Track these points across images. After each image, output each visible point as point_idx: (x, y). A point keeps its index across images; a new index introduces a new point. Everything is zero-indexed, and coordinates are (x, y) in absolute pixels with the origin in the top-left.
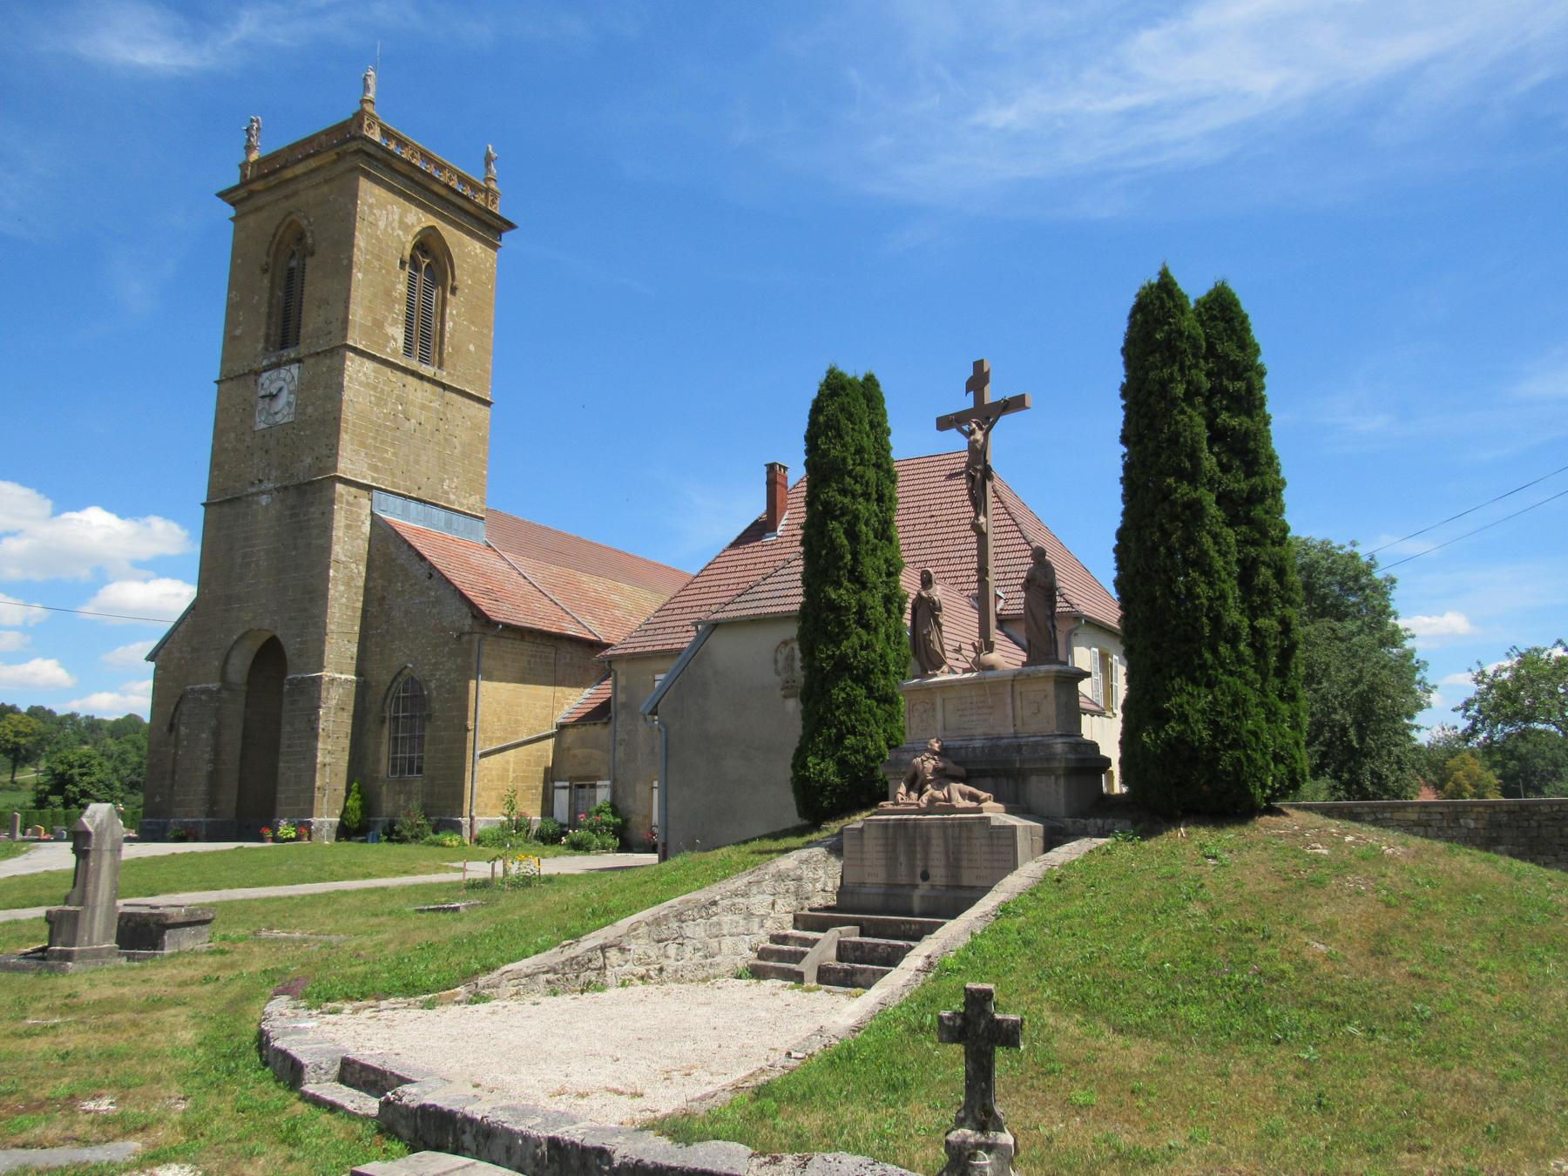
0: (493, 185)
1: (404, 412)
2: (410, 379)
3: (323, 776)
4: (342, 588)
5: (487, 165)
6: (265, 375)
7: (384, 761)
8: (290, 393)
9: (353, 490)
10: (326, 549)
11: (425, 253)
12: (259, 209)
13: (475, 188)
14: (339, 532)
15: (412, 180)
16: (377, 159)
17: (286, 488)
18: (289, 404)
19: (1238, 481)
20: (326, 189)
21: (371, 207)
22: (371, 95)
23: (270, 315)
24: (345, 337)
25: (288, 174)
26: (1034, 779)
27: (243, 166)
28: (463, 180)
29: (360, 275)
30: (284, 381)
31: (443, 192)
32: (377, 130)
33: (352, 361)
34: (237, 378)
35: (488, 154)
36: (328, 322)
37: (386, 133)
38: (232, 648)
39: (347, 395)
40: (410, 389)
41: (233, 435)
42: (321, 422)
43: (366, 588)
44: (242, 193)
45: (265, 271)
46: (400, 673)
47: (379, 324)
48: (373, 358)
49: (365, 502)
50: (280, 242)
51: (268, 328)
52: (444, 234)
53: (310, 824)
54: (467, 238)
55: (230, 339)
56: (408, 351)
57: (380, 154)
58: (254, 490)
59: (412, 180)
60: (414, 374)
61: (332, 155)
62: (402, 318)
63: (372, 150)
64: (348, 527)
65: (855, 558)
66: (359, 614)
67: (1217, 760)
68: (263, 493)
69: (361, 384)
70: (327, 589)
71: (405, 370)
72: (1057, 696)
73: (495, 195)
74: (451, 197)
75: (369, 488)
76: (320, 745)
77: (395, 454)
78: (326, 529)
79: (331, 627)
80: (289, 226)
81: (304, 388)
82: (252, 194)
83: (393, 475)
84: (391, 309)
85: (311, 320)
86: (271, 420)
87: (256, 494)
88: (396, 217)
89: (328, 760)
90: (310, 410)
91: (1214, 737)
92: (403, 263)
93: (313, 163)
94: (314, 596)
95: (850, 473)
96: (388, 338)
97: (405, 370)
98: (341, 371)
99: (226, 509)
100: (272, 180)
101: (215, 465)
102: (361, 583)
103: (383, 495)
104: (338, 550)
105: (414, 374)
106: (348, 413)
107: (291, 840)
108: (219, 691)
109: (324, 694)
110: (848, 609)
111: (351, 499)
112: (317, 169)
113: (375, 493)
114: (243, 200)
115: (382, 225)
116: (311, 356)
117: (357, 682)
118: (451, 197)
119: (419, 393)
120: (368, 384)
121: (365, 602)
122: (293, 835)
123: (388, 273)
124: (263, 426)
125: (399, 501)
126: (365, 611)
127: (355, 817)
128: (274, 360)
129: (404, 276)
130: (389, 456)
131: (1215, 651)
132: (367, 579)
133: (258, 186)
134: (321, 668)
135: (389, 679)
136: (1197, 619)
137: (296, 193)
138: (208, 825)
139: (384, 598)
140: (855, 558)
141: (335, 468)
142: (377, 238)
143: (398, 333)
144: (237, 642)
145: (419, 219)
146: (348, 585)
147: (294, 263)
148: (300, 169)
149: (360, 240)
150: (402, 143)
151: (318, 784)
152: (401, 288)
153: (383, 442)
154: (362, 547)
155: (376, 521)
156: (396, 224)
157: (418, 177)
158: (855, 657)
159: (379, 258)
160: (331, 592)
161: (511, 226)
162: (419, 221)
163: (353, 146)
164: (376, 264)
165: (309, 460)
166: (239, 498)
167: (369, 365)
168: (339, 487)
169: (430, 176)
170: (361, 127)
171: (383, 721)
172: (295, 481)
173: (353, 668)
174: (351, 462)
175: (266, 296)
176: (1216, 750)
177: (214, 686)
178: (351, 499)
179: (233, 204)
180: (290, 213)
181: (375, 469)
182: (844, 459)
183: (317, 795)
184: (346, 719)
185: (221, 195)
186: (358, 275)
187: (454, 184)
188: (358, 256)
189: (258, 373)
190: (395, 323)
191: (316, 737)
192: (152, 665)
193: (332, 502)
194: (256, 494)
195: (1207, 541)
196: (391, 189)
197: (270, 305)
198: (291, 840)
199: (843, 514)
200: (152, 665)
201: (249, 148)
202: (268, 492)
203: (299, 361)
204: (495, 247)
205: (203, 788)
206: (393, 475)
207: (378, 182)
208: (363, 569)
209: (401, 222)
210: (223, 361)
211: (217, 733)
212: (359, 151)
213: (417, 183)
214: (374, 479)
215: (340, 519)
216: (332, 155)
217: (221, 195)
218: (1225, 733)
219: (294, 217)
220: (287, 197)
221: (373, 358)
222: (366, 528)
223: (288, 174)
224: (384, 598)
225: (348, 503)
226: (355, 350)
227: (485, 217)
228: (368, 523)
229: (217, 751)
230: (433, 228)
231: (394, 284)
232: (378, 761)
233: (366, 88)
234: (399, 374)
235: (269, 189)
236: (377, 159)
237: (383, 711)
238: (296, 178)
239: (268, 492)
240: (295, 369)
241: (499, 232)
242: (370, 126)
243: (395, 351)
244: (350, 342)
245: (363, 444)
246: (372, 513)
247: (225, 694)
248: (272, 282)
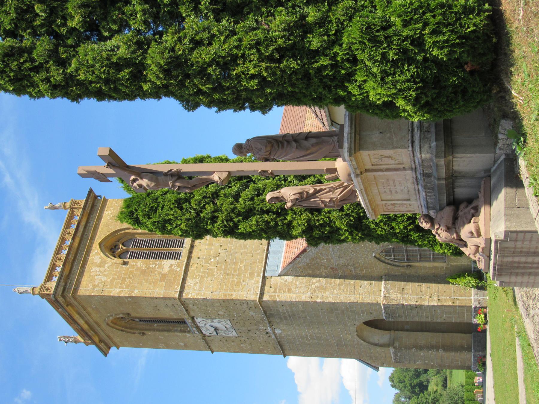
0: (68, 205)
1: (215, 257)
2: (194, 254)
3: (446, 300)
4: (328, 293)
5: (56, 208)
6: (204, 332)
7: (436, 264)
8: (212, 321)
9: (266, 289)
10: (305, 304)
11: (116, 247)
12: (109, 337)
13: (71, 216)
14: (293, 297)
15: (74, 260)
16: (66, 284)
17: (270, 322)
18: (219, 322)
19: (134, 14)
20: (89, 309)
21: (94, 286)
22: (30, 290)
23: (169, 331)
24: (174, 299)
25: (85, 327)
26: (456, 196)
27: (87, 344)
28: (68, 225)
29: (136, 291)
30: (206, 325)
31: (77, 240)
32: (49, 284)
33: (188, 293)
34: (208, 344)
35: (50, 208)
36: (167, 306)
37: (49, 278)
38: (369, 343)
39: (209, 296)
40: (200, 254)
41: (242, 345)
42: (228, 307)
43: (326, 277)
44: (102, 345)
45: (144, 334)
46: (379, 259)
47: (164, 277)
48: (184, 280)
49: (273, 281)
50: (125, 327)
51: (176, 331)
52: (103, 237)
53: (475, 307)
54: (103, 221)
55: (186, 347)
56: (176, 256)
57: (62, 284)
58: (273, 337)
59: (74, 260)
60: (190, 252)
61: (69, 309)
62: (158, 262)
63: (61, 289)
64: (289, 291)
65: (268, 212)
66: (343, 281)
67: (435, 60)
68: (274, 332)
69: (202, 288)
70: (328, 302)
71: (189, 258)
72: (374, 146)
73: (74, 203)
74: (79, 234)
75: (264, 278)
76: (426, 303)
77: (242, 262)
78: (292, 304)
79: (352, 299)
80: (116, 324)
81: (207, 315)
82: (101, 341)
83: (255, 262)
84: (153, 270)
85: (167, 313)
86: (231, 329)
87: (275, 335)
88: (98, 269)
89: (436, 298)
90: (220, 313)
91: (411, 61)
92: (125, 263)
93: (76, 316)
94: (334, 310)
95: (198, 214)
96: (171, 271)
97: (189, 258)
98: (195, 301)
99: (286, 347)
100: (91, 333)
101: (261, 352)
102: (323, 280)
103: (268, 268)
104: (305, 297)
105: (190, 252)
106: (219, 294)
107: (486, 316)
108: (394, 348)
109: (394, 302)
110: (309, 221)
111: (272, 290)
112: (79, 314)
113: (267, 274)
114: (106, 344)
115: (104, 279)
116: (189, 314)
117: (386, 280)
118: (79, 234)
119: (202, 248)
120: (201, 282)
121: (335, 277)
122: (482, 316)
123: (131, 272)
124: (234, 332)
125: (270, 257)
126: (341, 277)
127: (473, 282)
128: (194, 329)
129: (132, 262)
130: (243, 266)
131: (316, 54)
132: (321, 277)
133: (96, 339)
134: (378, 304)
135: (382, 264)
136: (283, 71)
137: (96, 323)
138: (476, 351)
139: (332, 268)
140: (268, 212)
141: (255, 301)
142: (112, 281)
143: (167, 264)
144: (364, 341)
145: (96, 255)
146: (325, 289)
147: (137, 320)
148: (81, 322)
149: (115, 292)
150: (53, 267)
151: (450, 304)
152: (140, 263)
153: (235, 270)
154: (301, 281)
155: (285, 273)
156: (102, 269)
157: (71, 257)
158: (348, 215)
159: (124, 279)
160: (331, 300)
161: (91, 191)
162: (97, 254)
163: (60, 299)
164: (128, 280)
165: (251, 313)
166: (279, 342)
167: (189, 282)
168: (266, 298)
169: (70, 247)
170: (49, 295)
171: (410, 266)
172: (265, 318)
173: (377, 283)
174: (249, 292)
175: (157, 333)
176: (425, 59)
177: (392, 350)
178: (272, 290)
179: (109, 348)
180: (108, 324)
181: (252, 274)
182: (188, 220)
183: (457, 304)
184: (410, 286)
185: (106, 355)
186: (136, 293)
187: (72, 230)
188: (125, 293)
189: (204, 336)
190: (161, 267)
191: (421, 306)
192: (381, 368)
193: (275, 302)
194: (275, 335)
195: (204, 55)
196: (81, 274)
197: (164, 330)
198: (486, 316)
199: (231, 220)
200: (381, 368)
201: (76, 341)
202: (274, 330)
203: (193, 318)
204: (105, 200)
205: (454, 354)
206: (255, 262)
207: (79, 282)
208: (315, 280)
209: (100, 266)
210: (200, 350)
211: (420, 348)
212: (63, 296)
213: (75, 257)
214: (259, 275)
215: (285, 297)
216: (69, 309)
217: (106, 355)
218: (405, 51)
219: (109, 322)
220: (99, 326)
221: (184, 280)
222: (289, 278)
223: (85, 327)
224: (332, 268)
225: (275, 292)
226: (181, 292)
227: (88, 210)
228: (286, 278)
229: (431, 347)
230: (100, 245)
231: (138, 269)
232: (435, 268)
233: (26, 292)
234: (192, 262)
235: (96, 333)
236: (66, 284)
237: (403, 266)
238: (87, 323)
239: (274, 330)
240: (197, 320)
241: (96, 197)
242: (47, 289)
243: (179, 265)
244: (177, 296)
245: (238, 283)
246: (280, 275)
247: (397, 344)
248: (150, 330)
